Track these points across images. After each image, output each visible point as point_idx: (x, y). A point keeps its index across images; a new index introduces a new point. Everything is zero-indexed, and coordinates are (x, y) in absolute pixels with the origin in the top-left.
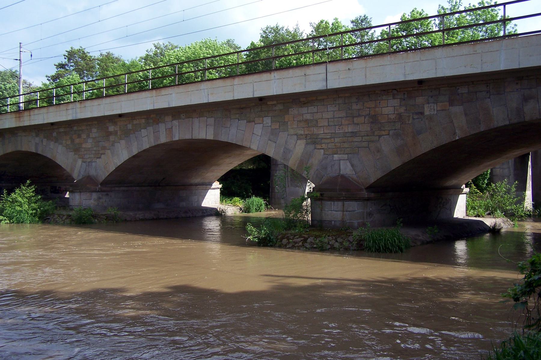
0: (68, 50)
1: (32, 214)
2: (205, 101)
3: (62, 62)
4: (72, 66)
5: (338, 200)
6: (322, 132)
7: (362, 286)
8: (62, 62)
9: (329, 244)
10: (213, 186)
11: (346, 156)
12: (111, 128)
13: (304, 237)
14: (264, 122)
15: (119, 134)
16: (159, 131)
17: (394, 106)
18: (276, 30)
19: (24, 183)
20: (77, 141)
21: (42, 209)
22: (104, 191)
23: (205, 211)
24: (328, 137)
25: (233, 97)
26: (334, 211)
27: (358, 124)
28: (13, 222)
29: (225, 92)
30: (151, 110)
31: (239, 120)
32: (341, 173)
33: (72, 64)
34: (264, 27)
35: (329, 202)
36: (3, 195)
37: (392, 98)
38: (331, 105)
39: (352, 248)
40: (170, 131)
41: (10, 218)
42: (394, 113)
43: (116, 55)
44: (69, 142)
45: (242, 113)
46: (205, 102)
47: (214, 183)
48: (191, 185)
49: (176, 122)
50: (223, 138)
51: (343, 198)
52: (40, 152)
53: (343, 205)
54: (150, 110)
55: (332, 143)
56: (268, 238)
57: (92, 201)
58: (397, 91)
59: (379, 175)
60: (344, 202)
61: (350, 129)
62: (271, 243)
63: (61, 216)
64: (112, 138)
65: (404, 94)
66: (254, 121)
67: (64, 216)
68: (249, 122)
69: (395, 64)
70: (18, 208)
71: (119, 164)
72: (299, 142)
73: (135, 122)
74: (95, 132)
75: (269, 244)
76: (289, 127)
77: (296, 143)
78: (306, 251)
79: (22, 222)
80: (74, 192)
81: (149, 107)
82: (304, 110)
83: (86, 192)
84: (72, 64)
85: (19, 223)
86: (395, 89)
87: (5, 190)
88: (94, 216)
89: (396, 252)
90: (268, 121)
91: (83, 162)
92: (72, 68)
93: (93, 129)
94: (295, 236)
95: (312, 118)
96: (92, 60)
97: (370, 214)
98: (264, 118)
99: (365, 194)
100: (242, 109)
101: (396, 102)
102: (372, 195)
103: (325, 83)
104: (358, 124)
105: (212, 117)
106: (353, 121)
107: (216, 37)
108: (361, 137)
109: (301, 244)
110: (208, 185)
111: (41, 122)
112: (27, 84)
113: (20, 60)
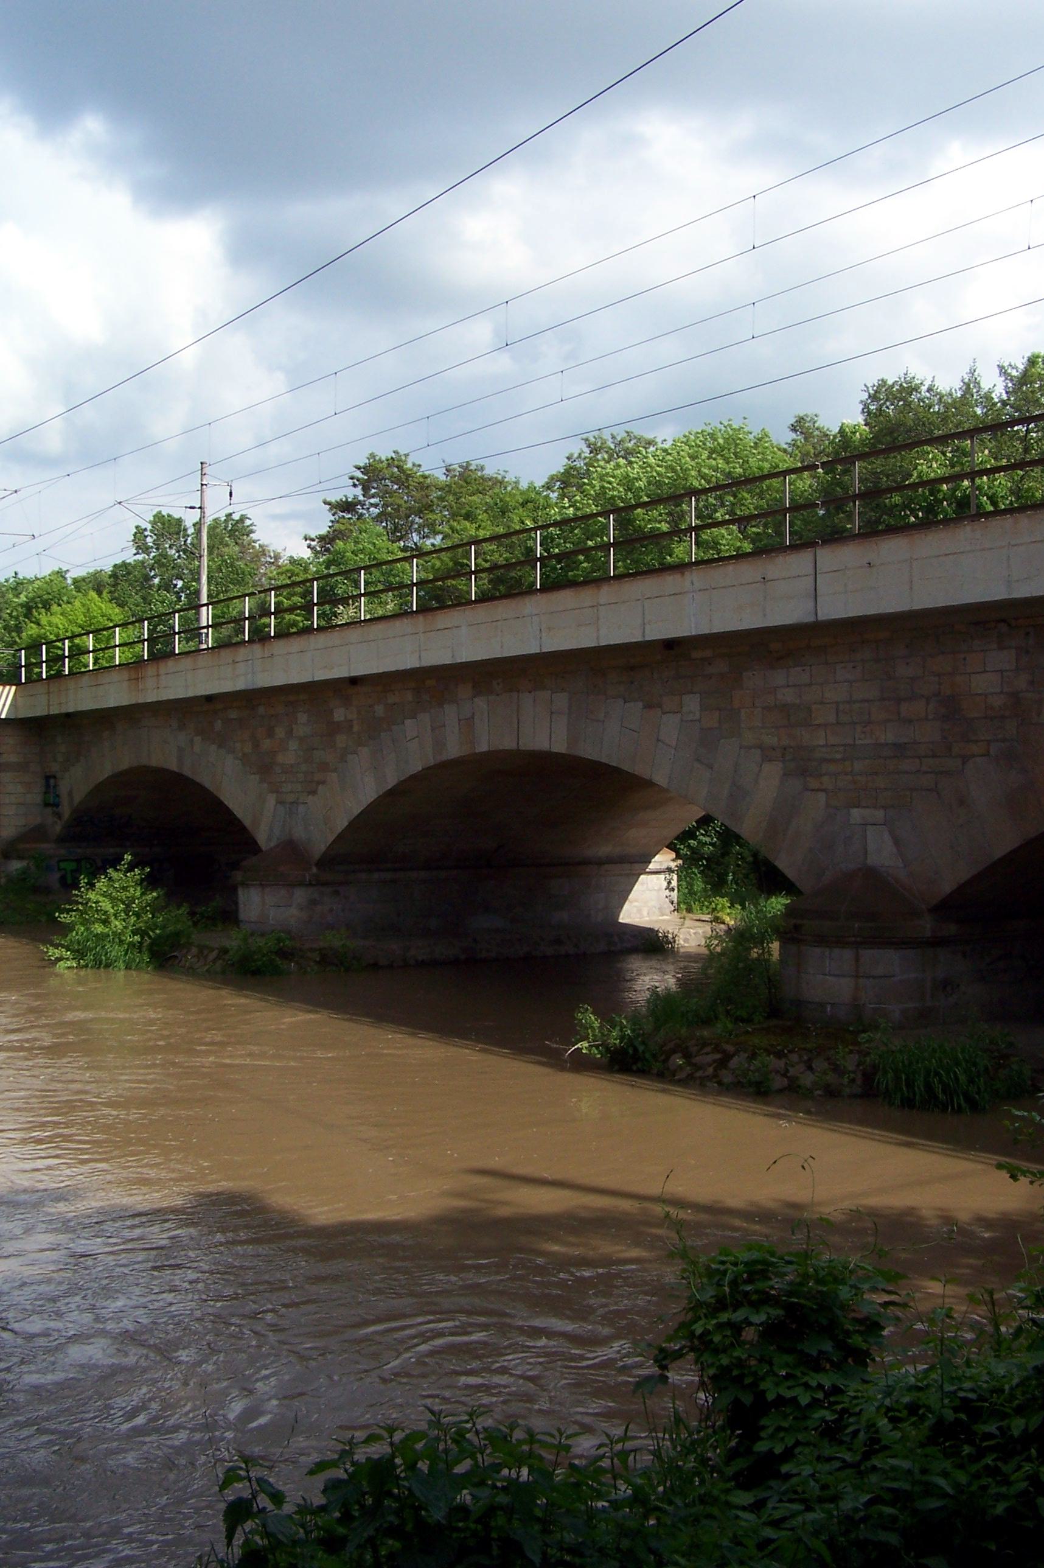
0: (362, 465)
1: (132, 945)
2: (534, 649)
3: (345, 496)
4: (376, 506)
5: (840, 942)
6: (822, 742)
7: (759, 1222)
8: (345, 496)
9: (787, 1077)
10: (652, 866)
11: (880, 814)
12: (339, 715)
13: (724, 1052)
14: (685, 709)
15: (356, 728)
16: (444, 726)
17: (1001, 671)
18: (906, 390)
19: (115, 862)
20: (266, 744)
21: (158, 931)
22: (326, 884)
23: (616, 939)
24: (838, 756)
25: (598, 638)
26: (830, 975)
27: (910, 721)
28: (86, 966)
29: (579, 625)
30: (414, 669)
31: (625, 702)
32: (869, 862)
33: (372, 501)
34: (873, 381)
35: (818, 950)
36: (79, 889)
37: (995, 646)
38: (843, 665)
39: (847, 1091)
40: (468, 724)
41: (79, 954)
42: (1002, 692)
43: (490, 471)
44: (248, 748)
45: (632, 683)
46: (533, 652)
47: (657, 857)
48: (586, 862)
49: (481, 703)
50: (589, 751)
51: (853, 939)
52: (187, 772)
53: (857, 960)
54: (410, 669)
55: (846, 774)
56: (631, 1051)
57: (294, 911)
58: (1009, 625)
59: (964, 872)
60: (860, 951)
61: (889, 736)
62: (639, 1065)
63: (206, 952)
64: (341, 740)
65: (1027, 634)
66: (660, 706)
67: (212, 950)
68: (649, 706)
69: (983, 550)
70: (99, 928)
71: (357, 811)
72: (767, 767)
73: (392, 699)
74: (303, 723)
75: (634, 1068)
76: (743, 725)
77: (760, 771)
78: (720, 1093)
79: (107, 966)
80: (247, 885)
81: (409, 662)
82: (779, 677)
83: (276, 885)
84: (372, 501)
85: (99, 968)
86: (1004, 621)
87: (82, 877)
88: (285, 954)
89: (960, 1110)
90: (692, 704)
91: (280, 802)
92: (374, 511)
93: (299, 715)
94: (704, 1045)
95: (798, 701)
96: (424, 485)
97: (946, 985)
98: (684, 697)
99: (926, 926)
100: (632, 668)
101: (1002, 659)
102: (952, 929)
103: (810, 605)
104: (910, 721)
105: (563, 690)
106: (899, 714)
107: (745, 418)
108: (917, 761)
109: (710, 1070)
110: (638, 863)
111: (181, 694)
112: (270, 556)
113: (200, 508)
